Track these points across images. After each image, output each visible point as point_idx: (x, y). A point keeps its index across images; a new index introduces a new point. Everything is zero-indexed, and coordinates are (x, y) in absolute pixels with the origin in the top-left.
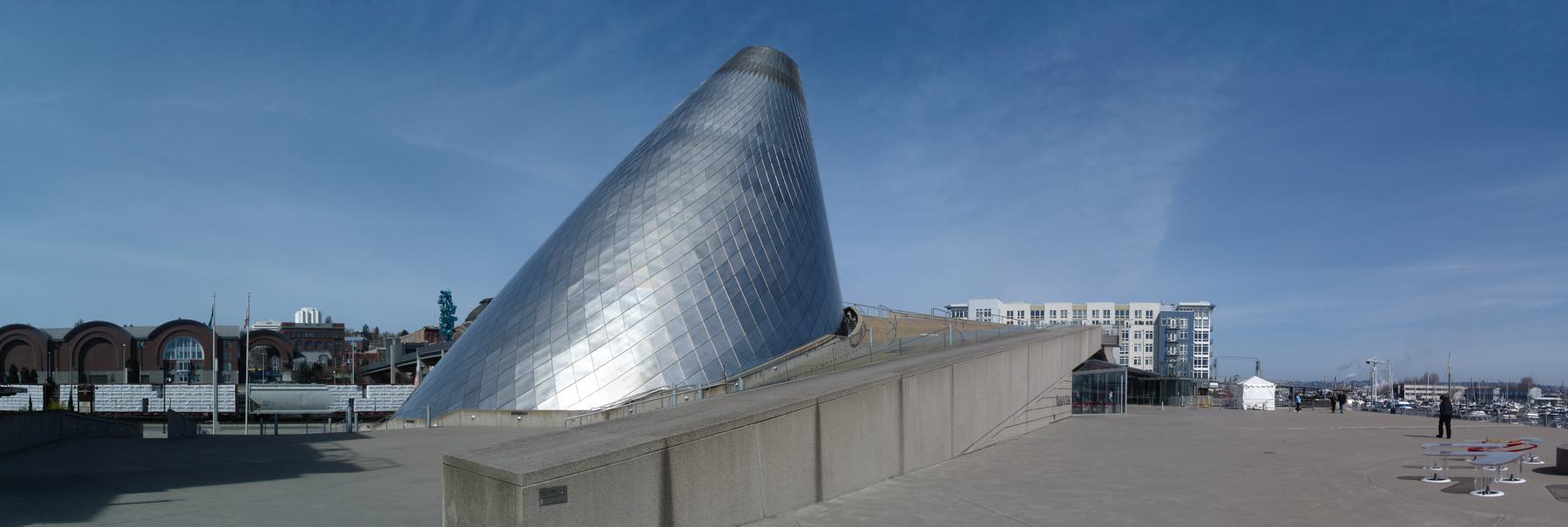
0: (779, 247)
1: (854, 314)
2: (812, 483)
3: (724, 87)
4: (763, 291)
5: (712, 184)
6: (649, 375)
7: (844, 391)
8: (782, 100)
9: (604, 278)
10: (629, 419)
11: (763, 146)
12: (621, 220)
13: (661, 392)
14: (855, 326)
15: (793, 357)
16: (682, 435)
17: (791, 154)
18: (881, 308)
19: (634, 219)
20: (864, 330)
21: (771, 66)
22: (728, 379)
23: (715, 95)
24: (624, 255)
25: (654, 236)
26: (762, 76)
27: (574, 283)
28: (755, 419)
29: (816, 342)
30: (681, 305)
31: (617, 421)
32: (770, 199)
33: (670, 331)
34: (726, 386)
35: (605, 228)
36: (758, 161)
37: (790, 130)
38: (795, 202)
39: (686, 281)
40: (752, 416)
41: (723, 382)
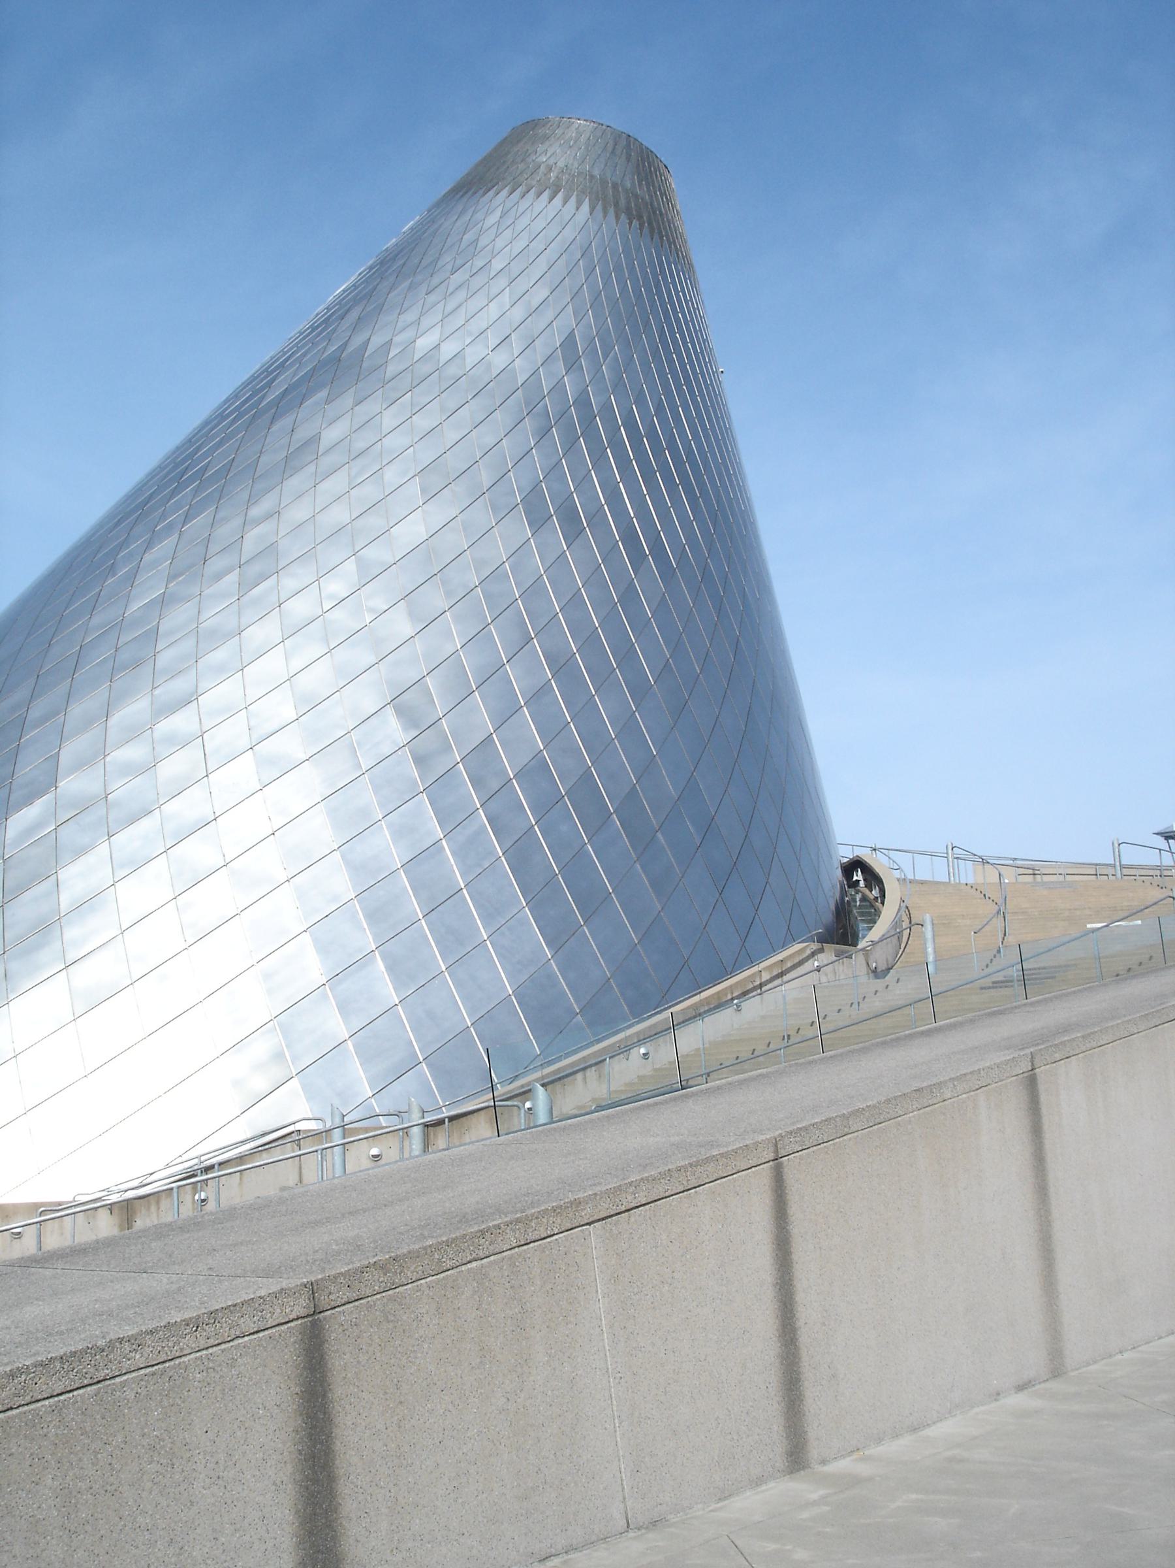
0: (640, 690)
1: (873, 878)
2: (771, 1410)
3: (469, 237)
4: (597, 823)
5: (439, 513)
6: (261, 1084)
7: (857, 1112)
8: (632, 269)
9: (123, 790)
10: (195, 1224)
11: (583, 402)
12: (177, 617)
13: (294, 1138)
14: (878, 913)
15: (696, 1015)
16: (362, 1270)
17: (663, 421)
18: (956, 856)
19: (215, 614)
20: (907, 924)
21: (596, 172)
22: (500, 1090)
23: (447, 258)
24: (181, 722)
25: (273, 665)
26: (573, 201)
27: (28, 800)
28: (587, 1213)
29: (764, 968)
30: (355, 868)
31: (161, 1232)
32: (610, 554)
33: (323, 949)
34: (495, 1111)
35: (126, 638)
36: (571, 446)
37: (655, 353)
38: (681, 556)
39: (367, 796)
40: (577, 1203)
41: (485, 1100)
